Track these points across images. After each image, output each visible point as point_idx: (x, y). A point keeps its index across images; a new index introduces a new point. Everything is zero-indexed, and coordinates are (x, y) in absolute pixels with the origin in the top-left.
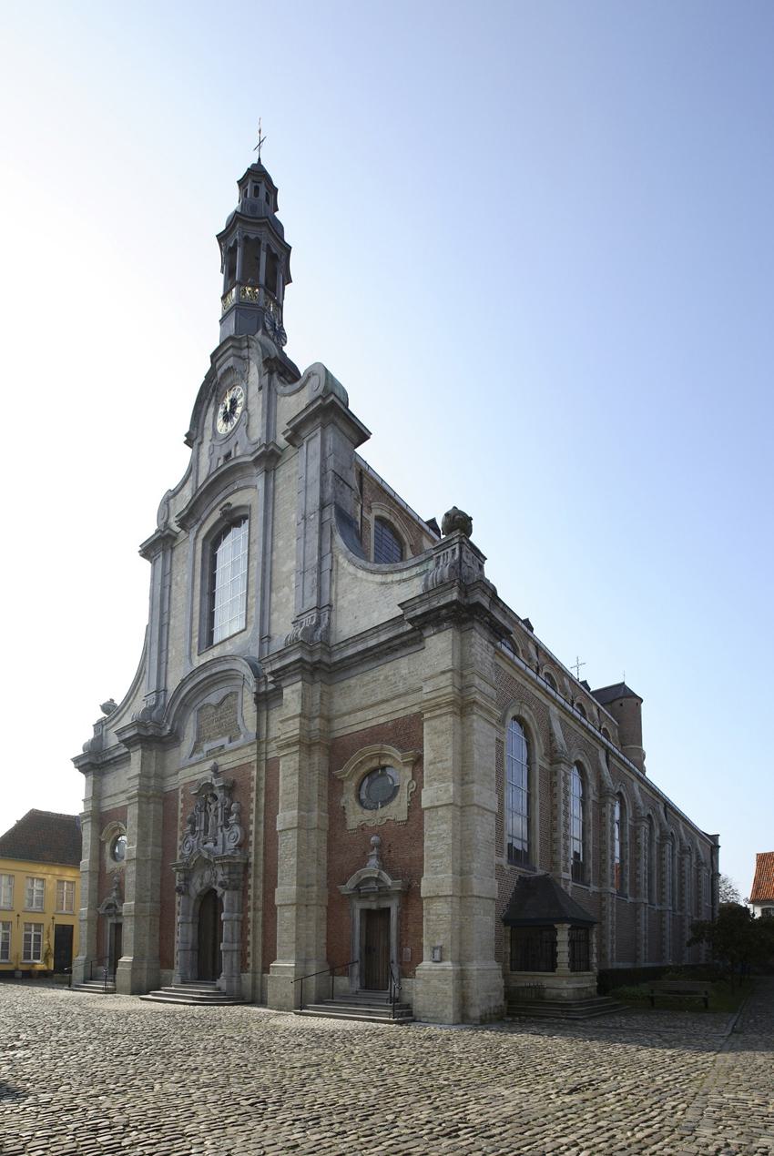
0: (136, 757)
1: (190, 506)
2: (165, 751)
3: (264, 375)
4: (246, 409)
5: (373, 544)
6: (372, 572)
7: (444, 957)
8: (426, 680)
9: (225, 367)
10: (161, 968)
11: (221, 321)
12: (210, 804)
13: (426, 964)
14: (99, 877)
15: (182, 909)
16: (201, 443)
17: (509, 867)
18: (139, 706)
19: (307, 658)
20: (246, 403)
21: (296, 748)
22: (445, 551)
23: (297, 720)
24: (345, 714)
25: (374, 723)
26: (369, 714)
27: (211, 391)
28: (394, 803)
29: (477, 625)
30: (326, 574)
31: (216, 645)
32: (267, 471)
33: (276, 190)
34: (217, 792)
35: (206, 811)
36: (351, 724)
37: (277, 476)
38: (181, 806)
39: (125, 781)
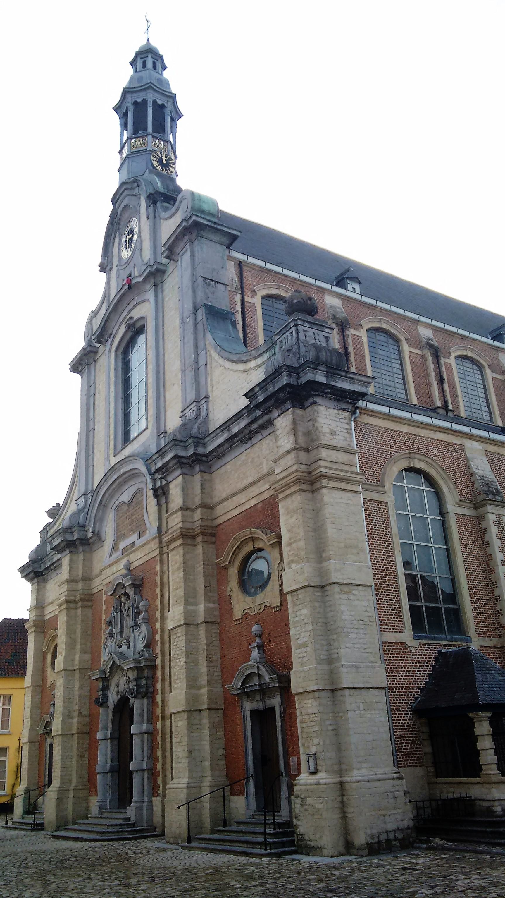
0: (66, 562)
1: (102, 325)
2: (92, 552)
3: (150, 206)
4: (139, 236)
5: (260, 323)
6: (236, 362)
7: (319, 768)
8: (276, 461)
9: (122, 206)
10: (231, 795)
11: (119, 170)
12: (124, 604)
13: (304, 778)
14: (42, 692)
15: (105, 716)
16: (111, 269)
17: (416, 643)
18: (73, 508)
19: (182, 453)
20: (140, 231)
21: (180, 542)
22: (290, 331)
23: (179, 513)
24: (223, 501)
25: (247, 506)
26: (241, 498)
27: (116, 225)
28: (268, 588)
29: (318, 400)
30: (202, 369)
31: (133, 441)
32: (156, 285)
33: (161, 57)
34: (128, 591)
35: (121, 611)
36: (227, 511)
37: (164, 287)
38: (104, 608)
39: (56, 589)
